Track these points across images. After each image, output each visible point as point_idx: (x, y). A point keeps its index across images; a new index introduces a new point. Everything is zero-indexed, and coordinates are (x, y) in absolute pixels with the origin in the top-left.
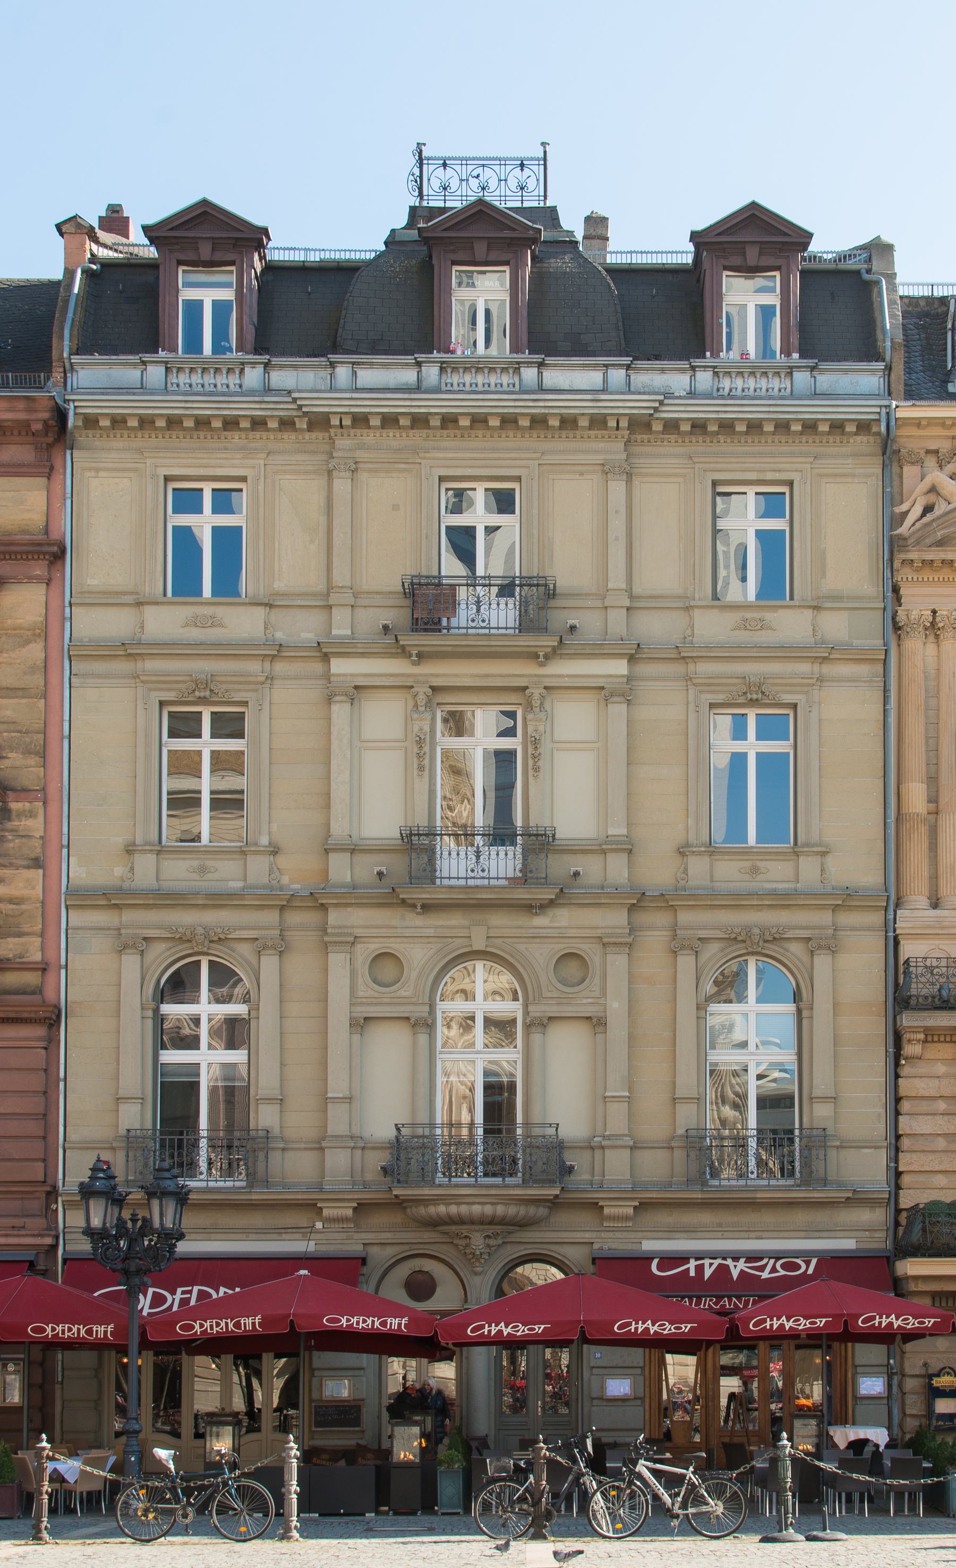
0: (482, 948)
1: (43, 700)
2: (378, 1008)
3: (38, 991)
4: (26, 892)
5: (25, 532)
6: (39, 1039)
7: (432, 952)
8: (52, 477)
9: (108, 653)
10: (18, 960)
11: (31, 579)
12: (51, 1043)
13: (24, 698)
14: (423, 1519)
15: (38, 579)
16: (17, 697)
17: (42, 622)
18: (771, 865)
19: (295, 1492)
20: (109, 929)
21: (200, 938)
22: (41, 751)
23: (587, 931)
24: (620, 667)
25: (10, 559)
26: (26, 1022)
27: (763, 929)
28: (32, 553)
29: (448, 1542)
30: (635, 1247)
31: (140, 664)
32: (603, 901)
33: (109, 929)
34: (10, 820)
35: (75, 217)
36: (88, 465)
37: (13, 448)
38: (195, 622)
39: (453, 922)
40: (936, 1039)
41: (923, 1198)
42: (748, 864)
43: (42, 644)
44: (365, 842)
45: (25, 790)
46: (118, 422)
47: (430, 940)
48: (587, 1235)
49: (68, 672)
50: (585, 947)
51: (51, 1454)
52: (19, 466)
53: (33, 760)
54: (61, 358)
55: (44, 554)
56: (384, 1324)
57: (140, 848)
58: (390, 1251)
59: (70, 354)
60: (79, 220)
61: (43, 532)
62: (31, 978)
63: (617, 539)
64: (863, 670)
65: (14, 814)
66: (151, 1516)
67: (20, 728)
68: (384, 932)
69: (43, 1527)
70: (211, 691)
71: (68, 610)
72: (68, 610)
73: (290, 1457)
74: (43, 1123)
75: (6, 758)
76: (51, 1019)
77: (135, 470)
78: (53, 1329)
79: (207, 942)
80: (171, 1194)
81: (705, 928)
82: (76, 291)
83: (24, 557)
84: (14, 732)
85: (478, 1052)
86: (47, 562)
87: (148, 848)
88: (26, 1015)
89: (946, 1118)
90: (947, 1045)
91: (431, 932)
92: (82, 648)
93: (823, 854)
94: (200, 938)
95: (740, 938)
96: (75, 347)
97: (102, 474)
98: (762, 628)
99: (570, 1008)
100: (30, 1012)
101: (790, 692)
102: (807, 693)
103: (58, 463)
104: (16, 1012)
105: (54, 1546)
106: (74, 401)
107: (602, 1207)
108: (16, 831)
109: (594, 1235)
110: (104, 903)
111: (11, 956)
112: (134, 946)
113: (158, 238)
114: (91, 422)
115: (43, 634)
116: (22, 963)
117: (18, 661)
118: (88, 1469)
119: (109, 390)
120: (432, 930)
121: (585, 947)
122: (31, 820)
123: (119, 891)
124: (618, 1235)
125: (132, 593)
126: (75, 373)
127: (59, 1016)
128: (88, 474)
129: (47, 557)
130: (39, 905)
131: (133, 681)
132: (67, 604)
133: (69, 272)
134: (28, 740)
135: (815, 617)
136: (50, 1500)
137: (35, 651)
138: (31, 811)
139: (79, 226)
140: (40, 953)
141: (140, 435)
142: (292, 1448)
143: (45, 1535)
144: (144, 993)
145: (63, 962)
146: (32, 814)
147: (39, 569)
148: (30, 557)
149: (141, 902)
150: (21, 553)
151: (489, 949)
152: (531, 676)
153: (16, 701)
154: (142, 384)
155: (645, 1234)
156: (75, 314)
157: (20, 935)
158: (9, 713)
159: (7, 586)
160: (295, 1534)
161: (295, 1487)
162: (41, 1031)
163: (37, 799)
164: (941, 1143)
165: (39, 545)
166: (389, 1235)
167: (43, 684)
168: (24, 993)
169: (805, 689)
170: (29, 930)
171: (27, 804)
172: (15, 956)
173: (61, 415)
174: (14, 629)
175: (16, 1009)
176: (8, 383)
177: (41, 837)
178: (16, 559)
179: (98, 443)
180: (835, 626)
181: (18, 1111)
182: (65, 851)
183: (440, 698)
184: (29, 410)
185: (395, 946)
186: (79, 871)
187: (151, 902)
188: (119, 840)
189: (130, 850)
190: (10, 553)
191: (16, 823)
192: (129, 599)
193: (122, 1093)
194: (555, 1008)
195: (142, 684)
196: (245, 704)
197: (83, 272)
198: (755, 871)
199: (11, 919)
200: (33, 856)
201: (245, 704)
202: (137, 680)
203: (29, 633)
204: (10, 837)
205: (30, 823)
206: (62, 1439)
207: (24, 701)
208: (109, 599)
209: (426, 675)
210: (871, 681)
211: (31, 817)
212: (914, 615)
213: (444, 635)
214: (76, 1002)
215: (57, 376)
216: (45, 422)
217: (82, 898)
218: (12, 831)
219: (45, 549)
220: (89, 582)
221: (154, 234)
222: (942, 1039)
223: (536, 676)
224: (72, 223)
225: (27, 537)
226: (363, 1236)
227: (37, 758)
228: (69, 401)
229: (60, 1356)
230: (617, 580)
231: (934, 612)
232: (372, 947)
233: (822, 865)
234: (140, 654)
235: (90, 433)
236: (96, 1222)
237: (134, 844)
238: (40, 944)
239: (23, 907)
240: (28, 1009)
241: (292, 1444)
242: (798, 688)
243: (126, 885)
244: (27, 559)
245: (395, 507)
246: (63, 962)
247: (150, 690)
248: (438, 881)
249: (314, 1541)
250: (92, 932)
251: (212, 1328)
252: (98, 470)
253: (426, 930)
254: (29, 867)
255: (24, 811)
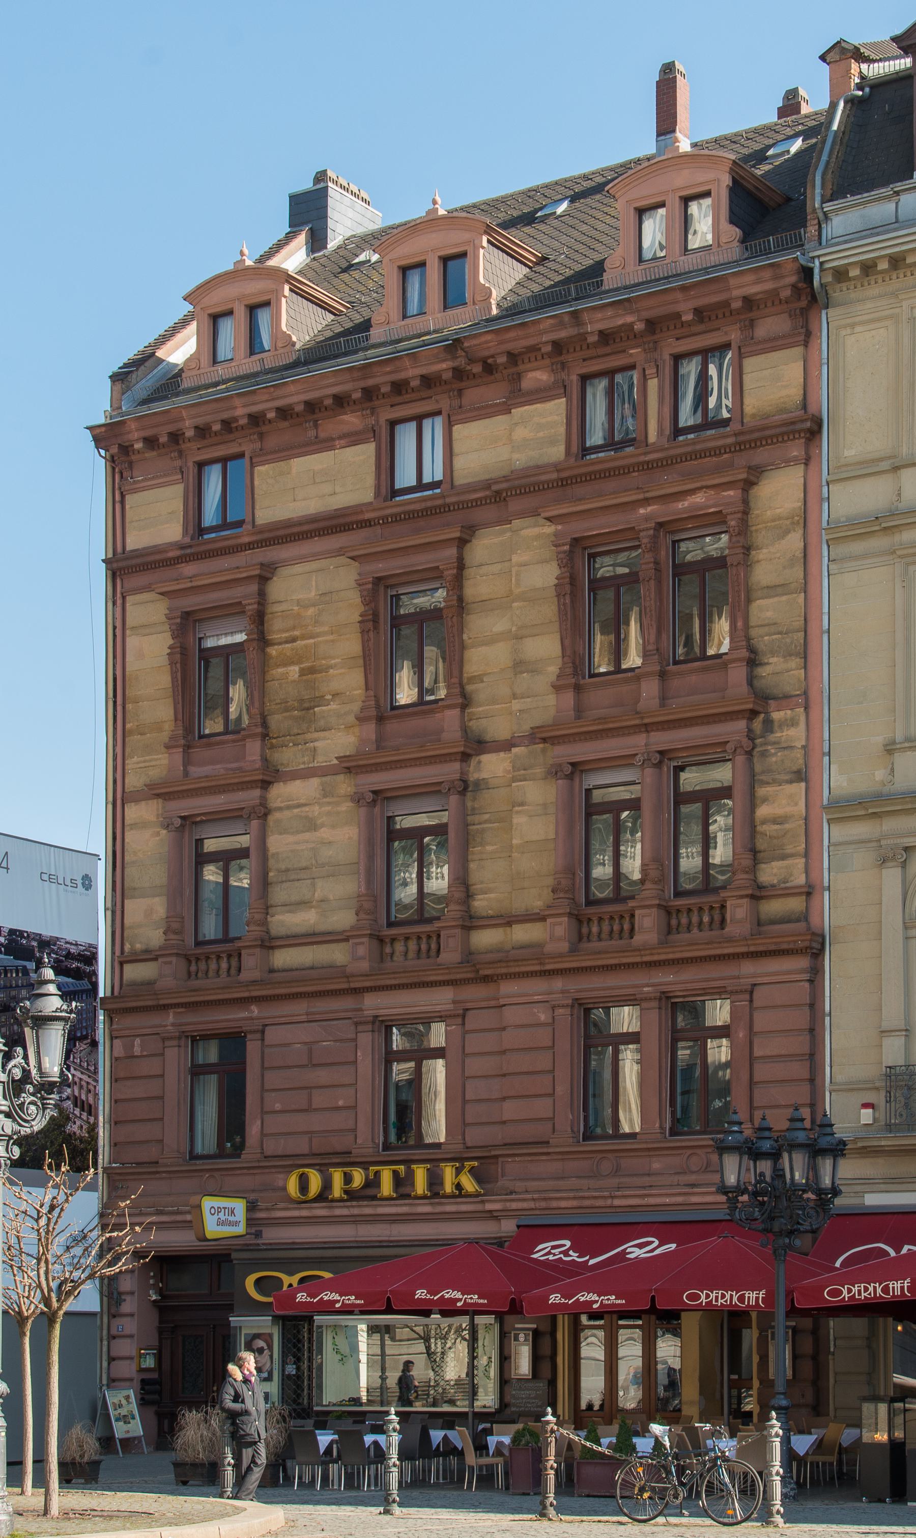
1: (803, 594)
3: (804, 917)
4: (789, 810)
5: (782, 411)
6: (801, 971)
8: (809, 345)
9: (863, 531)
10: (783, 885)
11: (789, 462)
12: (815, 975)
13: (783, 595)
14: (888, 1507)
15: (795, 461)
16: (777, 595)
17: (800, 507)
19: (778, 1474)
20: (870, 841)
22: (802, 651)
25: (767, 444)
26: (788, 954)
28: (787, 433)
29: (599, 1521)
31: (897, 538)
33: (870, 841)
34: (772, 732)
35: (838, 42)
36: (843, 322)
37: (769, 320)
43: (801, 532)
45: (787, 697)
46: (868, 268)
49: (826, 558)
51: (555, 1427)
52: (775, 339)
53: (795, 662)
54: (814, 210)
55: (799, 432)
56: (886, 1290)
57: (898, 746)
59: (823, 202)
60: (843, 44)
61: (800, 407)
62: (795, 904)
65: (776, 724)
66: (646, 1495)
67: (780, 629)
69: (548, 1504)
71: (825, 489)
72: (825, 489)
73: (771, 1436)
74: (808, 1064)
75: (768, 664)
76: (814, 948)
77: (890, 317)
78: (708, 1296)
80: (801, 1146)
82: (835, 127)
83: (780, 439)
84: (775, 634)
86: (803, 440)
87: (907, 745)
88: (785, 946)
92: (837, 530)
96: (829, 192)
97: (858, 329)
100: (789, 942)
103: (813, 327)
104: (776, 943)
105: (558, 1523)
106: (819, 257)
108: (778, 743)
110: (862, 812)
111: (775, 882)
112: (894, 858)
113: (910, 46)
114: (841, 274)
115: (802, 521)
116: (786, 888)
117: (778, 555)
118: (588, 1444)
119: (864, 233)
122: (792, 729)
123: (878, 798)
125: (890, 458)
126: (829, 222)
127: (823, 944)
128: (843, 333)
129: (802, 435)
130: (802, 822)
131: (891, 557)
132: (824, 483)
133: (833, 106)
134: (788, 640)
136: (556, 1475)
137: (794, 541)
138: (792, 719)
139: (844, 51)
140: (804, 875)
141: (894, 277)
142: (772, 1426)
143: (551, 1512)
144: (907, 910)
145: (826, 884)
146: (793, 723)
147: (796, 450)
148: (786, 438)
149: (899, 808)
150: (777, 436)
153: (776, 599)
154: (897, 217)
156: (830, 156)
157: (784, 857)
158: (769, 614)
159: (766, 474)
160: (778, 1519)
161: (777, 1468)
162: (803, 962)
163: (798, 705)
165: (793, 423)
167: (802, 576)
168: (789, 921)
170: (793, 851)
171: (789, 712)
172: (779, 882)
173: (807, 273)
174: (773, 521)
175: (774, 940)
176: (770, 249)
177: (804, 747)
178: (773, 443)
179: (853, 295)
181: (783, 1052)
182: (826, 759)
184: (776, 278)
186: (838, 780)
187: (909, 806)
188: (879, 740)
189: (890, 749)
190: (766, 438)
191: (778, 735)
192: (885, 465)
193: (885, 1025)
195: (899, 560)
197: (846, 103)
199: (775, 841)
200: (795, 769)
202: (894, 556)
203: (788, 522)
204: (773, 751)
205: (792, 732)
206: (835, 1417)
207: (784, 598)
208: (867, 469)
211: (793, 725)
214: (839, 927)
215: (812, 230)
216: (794, 286)
217: (848, 808)
218: (774, 743)
219: (799, 426)
220: (847, 453)
221: (904, 44)
224: (837, 49)
225: (784, 416)
227: (798, 660)
228: (813, 258)
229: (831, 1323)
234: (896, 526)
235: (844, 286)
236: (731, 1179)
237: (894, 742)
238: (803, 865)
239: (787, 826)
240: (786, 939)
241: (774, 1422)
243: (886, 790)
244: (783, 441)
246: (826, 884)
247: (908, 564)
249: (492, 1516)
250: (853, 846)
251: (860, 1294)
252: (853, 326)
254: (791, 782)
255: (786, 720)
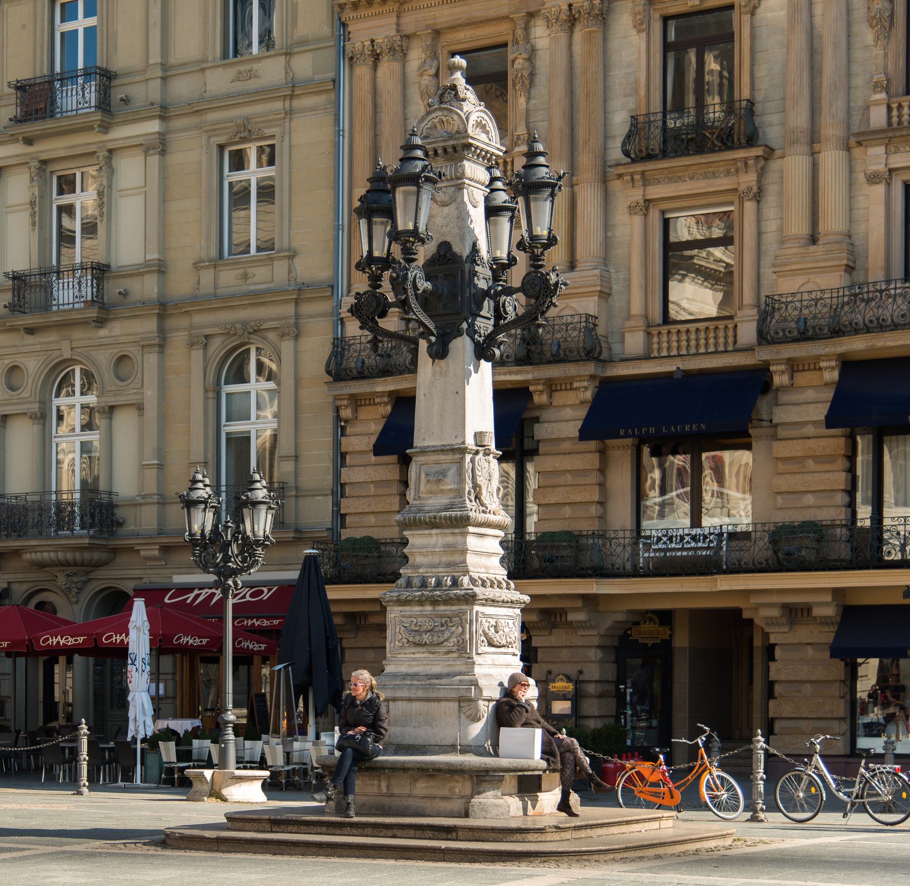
0: (69, 357)
2: (9, 408)
7: (41, 362)
18: (256, 270)
21: (240, 332)
23: (132, 337)
24: (154, 126)
27: (245, 324)
30: (168, 580)
32: (137, 313)
38: (238, 78)
39: (52, 339)
40: (367, 402)
41: (358, 534)
42: (240, 271)
44: (121, 269)
47: (40, 353)
48: (138, 572)
50: (132, 349)
58: (25, 587)
63: (155, 23)
64: (321, 99)
68: (12, 350)
70: (249, 131)
73: (757, 749)
79: (246, 334)
81: (208, 326)
85: (77, 435)
89: (374, 468)
90: (368, 407)
91: (38, 348)
93: (291, 258)
94: (240, 332)
95: (231, 333)
98: (250, 78)
99: (122, 398)
101: (269, 127)
102: (280, 126)
107: (139, 551)
109: (142, 572)
120: (39, 347)
121: (132, 349)
124: (157, 571)
135: (288, 63)
142: (759, 741)
151: (74, 357)
152: (98, 142)
155: (175, 570)
164: (372, 489)
166: (21, 575)
169: (279, 122)
180: (303, 65)
183: (51, 168)
185: (19, 360)
194: (112, 399)
196: (273, 137)
198: (245, 276)
201: (273, 137)
209: (36, 153)
210: (326, 108)
212: (358, 45)
213: (59, 118)
222: (558, 388)
223: (101, 142)
226: (7, 576)
230: (155, 57)
231: (373, 41)
232: (6, 362)
233: (289, 266)
241: (760, 738)
242: (275, 123)
245: (24, 27)
248: (55, 308)
253: (35, 347)
